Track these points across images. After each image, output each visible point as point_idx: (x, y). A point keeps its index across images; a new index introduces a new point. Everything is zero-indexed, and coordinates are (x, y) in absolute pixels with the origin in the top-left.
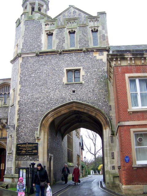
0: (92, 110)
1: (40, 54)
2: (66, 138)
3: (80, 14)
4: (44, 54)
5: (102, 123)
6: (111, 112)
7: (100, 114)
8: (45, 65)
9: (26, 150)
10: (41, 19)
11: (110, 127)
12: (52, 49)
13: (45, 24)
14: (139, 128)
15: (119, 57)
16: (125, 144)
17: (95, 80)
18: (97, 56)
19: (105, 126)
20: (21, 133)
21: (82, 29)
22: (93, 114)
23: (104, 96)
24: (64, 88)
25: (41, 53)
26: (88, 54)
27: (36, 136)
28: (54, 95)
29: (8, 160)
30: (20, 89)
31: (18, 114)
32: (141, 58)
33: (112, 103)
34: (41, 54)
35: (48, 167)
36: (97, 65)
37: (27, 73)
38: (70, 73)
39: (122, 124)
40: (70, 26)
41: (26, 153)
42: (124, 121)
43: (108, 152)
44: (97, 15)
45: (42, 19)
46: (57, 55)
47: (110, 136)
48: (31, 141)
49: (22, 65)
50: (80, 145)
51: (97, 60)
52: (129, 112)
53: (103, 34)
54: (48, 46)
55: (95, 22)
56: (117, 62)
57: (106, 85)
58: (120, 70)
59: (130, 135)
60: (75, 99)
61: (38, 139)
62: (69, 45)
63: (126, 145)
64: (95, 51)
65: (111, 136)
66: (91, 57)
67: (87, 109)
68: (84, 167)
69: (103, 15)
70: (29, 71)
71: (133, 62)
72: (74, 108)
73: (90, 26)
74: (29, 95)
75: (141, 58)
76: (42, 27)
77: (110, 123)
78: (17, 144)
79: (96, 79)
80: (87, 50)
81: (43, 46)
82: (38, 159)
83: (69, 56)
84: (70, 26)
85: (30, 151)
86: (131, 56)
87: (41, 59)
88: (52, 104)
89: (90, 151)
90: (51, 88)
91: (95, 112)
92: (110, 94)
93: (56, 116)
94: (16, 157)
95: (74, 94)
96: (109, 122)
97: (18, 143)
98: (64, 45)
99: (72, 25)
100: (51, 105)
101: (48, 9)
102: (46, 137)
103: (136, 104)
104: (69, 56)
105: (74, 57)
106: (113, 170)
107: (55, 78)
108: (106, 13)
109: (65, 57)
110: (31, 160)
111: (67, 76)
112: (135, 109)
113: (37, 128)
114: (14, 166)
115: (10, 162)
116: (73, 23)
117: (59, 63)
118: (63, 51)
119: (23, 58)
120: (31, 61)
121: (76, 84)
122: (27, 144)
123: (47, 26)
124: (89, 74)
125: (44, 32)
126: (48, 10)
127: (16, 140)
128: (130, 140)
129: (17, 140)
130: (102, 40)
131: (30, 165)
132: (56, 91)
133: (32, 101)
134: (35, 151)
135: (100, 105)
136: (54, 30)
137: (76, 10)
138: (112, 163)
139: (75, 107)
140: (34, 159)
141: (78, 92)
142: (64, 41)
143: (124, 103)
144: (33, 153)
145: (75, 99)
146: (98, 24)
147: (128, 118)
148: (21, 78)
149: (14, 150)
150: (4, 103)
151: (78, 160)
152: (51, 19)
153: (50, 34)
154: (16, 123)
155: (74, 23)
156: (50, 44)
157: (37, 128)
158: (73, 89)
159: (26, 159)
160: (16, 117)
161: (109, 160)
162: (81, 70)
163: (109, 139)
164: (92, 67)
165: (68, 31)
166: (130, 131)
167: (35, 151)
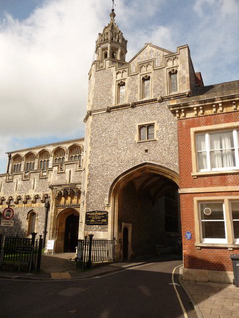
3: (158, 53)
13: (116, 72)
49: (92, 125)
52: (193, 176)
58: (184, 124)
72: (148, 171)
79: (172, 134)
94: (85, 226)
102: (117, 204)
105: (147, 109)
112: (203, 172)
124: (164, 129)
134: (105, 220)
141: (151, 151)
148: (91, 139)
162: (156, 125)
167: (105, 220)
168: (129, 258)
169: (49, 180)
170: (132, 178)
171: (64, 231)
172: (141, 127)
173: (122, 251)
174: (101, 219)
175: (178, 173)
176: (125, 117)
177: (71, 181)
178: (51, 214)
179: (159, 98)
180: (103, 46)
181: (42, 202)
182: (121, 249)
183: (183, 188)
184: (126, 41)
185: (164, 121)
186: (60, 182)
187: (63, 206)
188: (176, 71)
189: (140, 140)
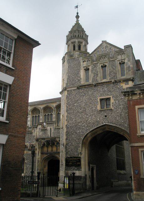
2: (114, 148)
4: (83, 87)
8: (84, 96)
9: (74, 162)
17: (122, 106)
21: (111, 63)
22: (122, 134)
27: (79, 151)
31: (66, 135)
35: (90, 176)
40: (102, 61)
48: (76, 155)
52: (138, 136)
54: (86, 80)
61: (81, 154)
62: (102, 78)
64: (122, 81)
72: (107, 129)
78: (66, 158)
84: (102, 61)
86: (140, 92)
94: (65, 167)
101: (88, 43)
102: (87, 152)
111: (101, 104)
116: (104, 58)
118: (97, 84)
119: (68, 91)
120: (74, 93)
121: (107, 110)
124: (117, 101)
131: (71, 174)
134: (79, 163)
140: (78, 169)
148: (67, 107)
149: (64, 162)
150: (57, 125)
152: (89, 54)
153: (87, 70)
155: (106, 58)
156: (87, 79)
160: (65, 137)
162: (111, 98)
164: (120, 95)
165: (101, 66)
167: (79, 163)
168: (95, 189)
169: (33, 134)
170: (96, 134)
171: (47, 171)
172: (101, 100)
173: (91, 184)
175: (128, 131)
177: (52, 135)
178: (38, 159)
179: (113, 81)
180: (73, 40)
181: (29, 150)
182: (90, 183)
183: (132, 143)
185: (117, 97)
186: (44, 136)
187: (47, 154)
188: (124, 62)
189: (101, 108)
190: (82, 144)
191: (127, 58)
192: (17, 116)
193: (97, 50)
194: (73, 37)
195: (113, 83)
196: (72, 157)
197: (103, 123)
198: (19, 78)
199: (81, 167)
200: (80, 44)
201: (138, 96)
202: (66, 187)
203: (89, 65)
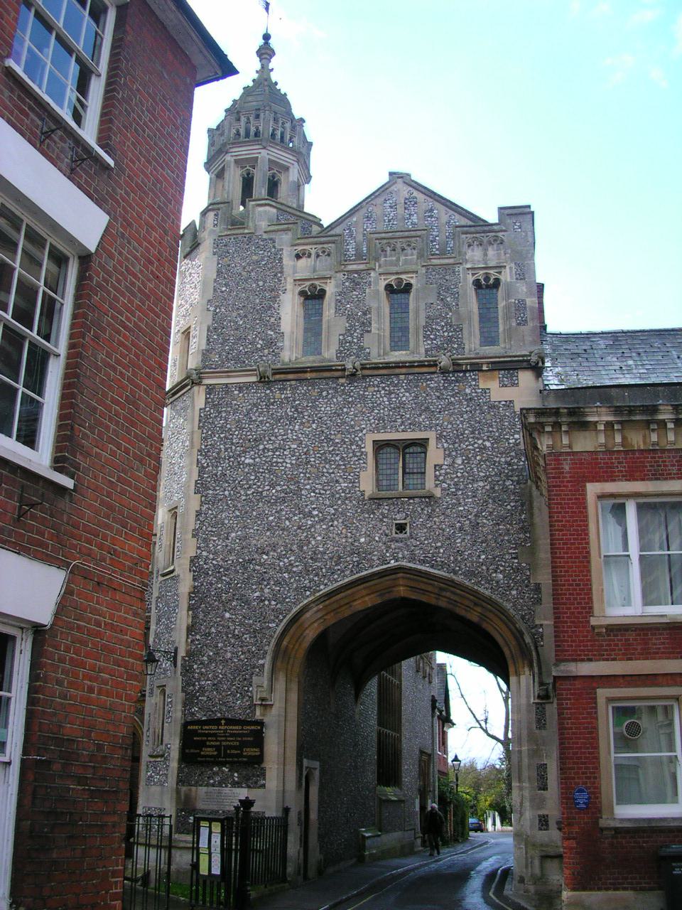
0: (467, 603)
1: (274, 374)
2: (372, 687)
3: (431, 210)
4: (291, 376)
5: (507, 652)
6: (538, 609)
7: (496, 615)
8: (292, 420)
9: (219, 745)
10: (278, 231)
11: (536, 670)
12: (320, 354)
14: (629, 685)
15: (564, 419)
16: (577, 743)
17: (481, 484)
18: (495, 389)
19: (514, 663)
20: (199, 680)
22: (474, 617)
23: (515, 549)
24: (362, 512)
25: (277, 372)
26: (457, 381)
28: (326, 537)
29: (150, 778)
30: (199, 514)
32: (648, 423)
33: (544, 578)
34: (278, 377)
35: (299, 813)
36: (492, 426)
37: (226, 450)
38: (389, 454)
39: (567, 671)
40: (392, 264)
41: (219, 756)
42: (575, 660)
43: (525, 761)
44: (497, 222)
45: (283, 230)
46: (342, 381)
47: (532, 701)
48: (238, 707)
50: (434, 707)
51: (492, 407)
52: (593, 627)
53: (520, 297)
55: (490, 249)
56: (558, 435)
57: (522, 505)
58: (567, 468)
59: (596, 713)
60: (403, 558)
63: (580, 748)
65: (537, 703)
66: (468, 391)
67: (448, 594)
68: (450, 803)
69: (520, 218)
70: (232, 444)
71: (671, 437)
72: (402, 591)
73: (469, 266)
74: (233, 535)
75: (648, 423)
76: (282, 268)
77: (534, 653)
78: (185, 725)
79: (485, 479)
80: (454, 364)
81: (287, 343)
82: (264, 779)
83: (383, 388)
84: (392, 264)
85: (233, 752)
86: (611, 418)
87: (277, 395)
88: (317, 575)
89: (483, 724)
90: (315, 513)
91: (479, 609)
92: (540, 542)
93: (331, 619)
94: (180, 770)
95: (401, 536)
96: (533, 648)
97: (189, 719)
98: (368, 341)
99: (398, 260)
100: (316, 578)
101: (308, 178)
102: (294, 697)
103: (627, 601)
104: (383, 388)
106: (540, 829)
107: (330, 474)
108: (533, 213)
109: (371, 389)
110: (237, 784)
113: (261, 662)
114: (174, 804)
115: (155, 789)
116: (403, 249)
117: (347, 413)
118: (363, 367)
119: (210, 389)
120: (243, 401)
121: (410, 498)
122: (223, 722)
123: (303, 262)
124: (459, 461)
125: (289, 286)
126: (308, 182)
127: (179, 707)
128: (596, 728)
129: (185, 705)
130: (514, 324)
132: (336, 523)
133: (244, 560)
134: (253, 751)
135: (497, 582)
136: (330, 278)
137: (416, 193)
138: (538, 803)
139: (402, 585)
142: (366, 325)
143: (577, 594)
144: (245, 757)
145: (403, 558)
146: (499, 255)
147: (589, 651)
148: (202, 470)
149: (174, 744)
151: (424, 772)
152: (321, 226)
153: (313, 296)
154: (180, 639)
155: (409, 251)
157: (261, 662)
158: (398, 516)
159: (217, 779)
160: (183, 618)
161: (526, 793)
162: (432, 444)
163: (529, 711)
164: (473, 432)
165: (383, 284)
166: (596, 698)
167: (253, 751)
172: (379, 446)
174: (240, 748)
176: (325, 408)
182: (301, 846)
184: (311, 144)
188: (497, 282)
190: (275, 659)
191: (513, 265)
192: (113, 454)
193: (363, 211)
194: (247, 135)
195: (444, 372)
196: (220, 719)
197: (385, 562)
198: (129, 224)
199: (264, 770)
200: (273, 177)
201: (602, 439)
202: (204, 870)
203: (328, 273)
